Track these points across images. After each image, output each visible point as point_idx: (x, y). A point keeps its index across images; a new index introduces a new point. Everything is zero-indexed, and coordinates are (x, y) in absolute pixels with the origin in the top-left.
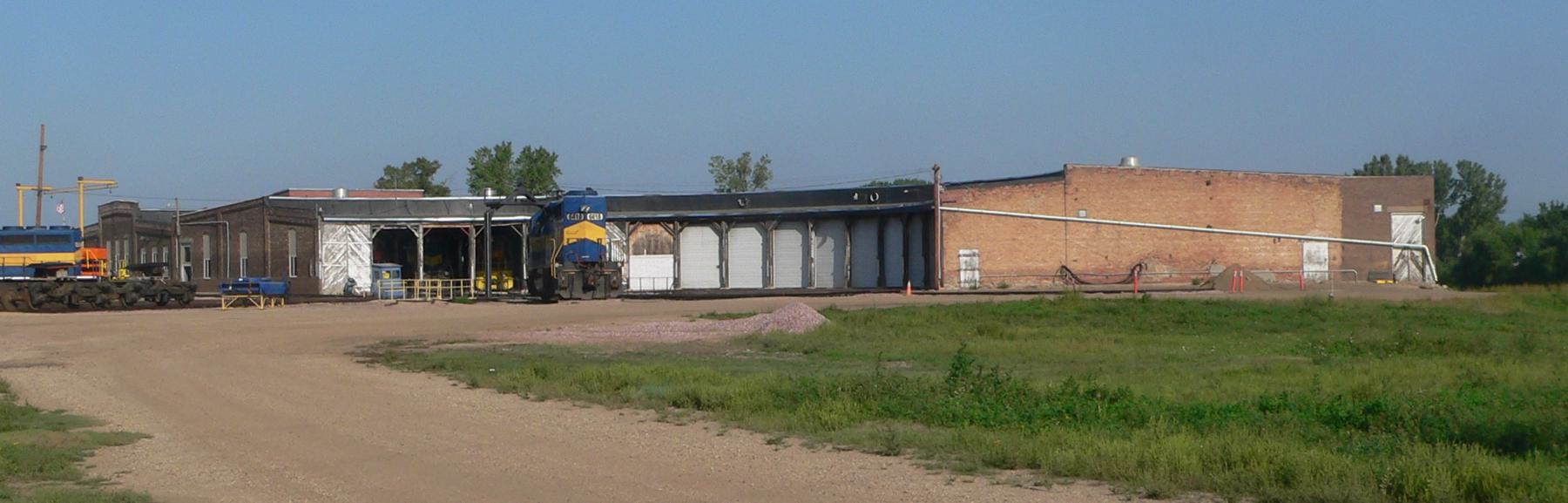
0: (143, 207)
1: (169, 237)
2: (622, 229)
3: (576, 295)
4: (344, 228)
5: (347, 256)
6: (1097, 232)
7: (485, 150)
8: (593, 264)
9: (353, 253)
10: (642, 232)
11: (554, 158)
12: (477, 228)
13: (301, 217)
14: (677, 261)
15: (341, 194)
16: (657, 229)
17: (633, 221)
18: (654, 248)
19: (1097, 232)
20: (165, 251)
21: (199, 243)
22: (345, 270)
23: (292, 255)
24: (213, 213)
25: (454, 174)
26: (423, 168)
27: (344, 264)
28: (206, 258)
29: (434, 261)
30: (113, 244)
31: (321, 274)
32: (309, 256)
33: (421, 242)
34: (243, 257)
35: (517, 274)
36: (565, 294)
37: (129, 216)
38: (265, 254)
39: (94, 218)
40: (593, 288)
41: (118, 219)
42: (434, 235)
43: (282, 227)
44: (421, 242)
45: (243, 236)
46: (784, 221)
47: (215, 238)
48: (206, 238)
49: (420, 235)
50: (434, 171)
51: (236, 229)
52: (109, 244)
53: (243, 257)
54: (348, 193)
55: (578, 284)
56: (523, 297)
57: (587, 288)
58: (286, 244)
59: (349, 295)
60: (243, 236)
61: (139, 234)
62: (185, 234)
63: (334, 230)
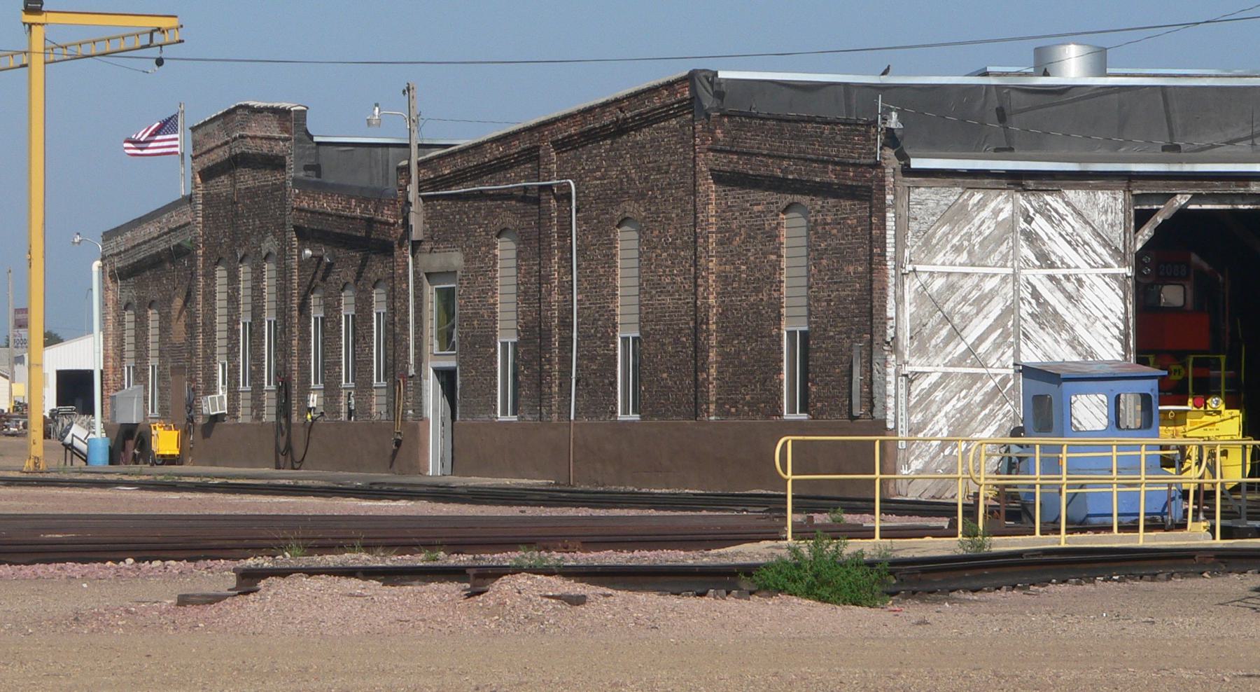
0: (323, 130)
1: (386, 249)
4: (1003, 205)
6: (1253, 144)
13: (829, 158)
15: (1072, 67)
19: (1253, 144)
20: (379, 300)
21: (482, 269)
23: (793, 323)
24: (523, 148)
28: (506, 336)
30: (233, 278)
31: (896, 406)
32: (853, 325)
34: (627, 330)
37: (275, 163)
38: (699, 320)
39: (180, 181)
41: (248, 179)
43: (761, 199)
45: (626, 242)
47: (534, 247)
48: (505, 250)
51: (604, 212)
52: (221, 273)
53: (627, 330)
60: (626, 242)
61: (305, 235)
62: (441, 235)
63: (957, 215)
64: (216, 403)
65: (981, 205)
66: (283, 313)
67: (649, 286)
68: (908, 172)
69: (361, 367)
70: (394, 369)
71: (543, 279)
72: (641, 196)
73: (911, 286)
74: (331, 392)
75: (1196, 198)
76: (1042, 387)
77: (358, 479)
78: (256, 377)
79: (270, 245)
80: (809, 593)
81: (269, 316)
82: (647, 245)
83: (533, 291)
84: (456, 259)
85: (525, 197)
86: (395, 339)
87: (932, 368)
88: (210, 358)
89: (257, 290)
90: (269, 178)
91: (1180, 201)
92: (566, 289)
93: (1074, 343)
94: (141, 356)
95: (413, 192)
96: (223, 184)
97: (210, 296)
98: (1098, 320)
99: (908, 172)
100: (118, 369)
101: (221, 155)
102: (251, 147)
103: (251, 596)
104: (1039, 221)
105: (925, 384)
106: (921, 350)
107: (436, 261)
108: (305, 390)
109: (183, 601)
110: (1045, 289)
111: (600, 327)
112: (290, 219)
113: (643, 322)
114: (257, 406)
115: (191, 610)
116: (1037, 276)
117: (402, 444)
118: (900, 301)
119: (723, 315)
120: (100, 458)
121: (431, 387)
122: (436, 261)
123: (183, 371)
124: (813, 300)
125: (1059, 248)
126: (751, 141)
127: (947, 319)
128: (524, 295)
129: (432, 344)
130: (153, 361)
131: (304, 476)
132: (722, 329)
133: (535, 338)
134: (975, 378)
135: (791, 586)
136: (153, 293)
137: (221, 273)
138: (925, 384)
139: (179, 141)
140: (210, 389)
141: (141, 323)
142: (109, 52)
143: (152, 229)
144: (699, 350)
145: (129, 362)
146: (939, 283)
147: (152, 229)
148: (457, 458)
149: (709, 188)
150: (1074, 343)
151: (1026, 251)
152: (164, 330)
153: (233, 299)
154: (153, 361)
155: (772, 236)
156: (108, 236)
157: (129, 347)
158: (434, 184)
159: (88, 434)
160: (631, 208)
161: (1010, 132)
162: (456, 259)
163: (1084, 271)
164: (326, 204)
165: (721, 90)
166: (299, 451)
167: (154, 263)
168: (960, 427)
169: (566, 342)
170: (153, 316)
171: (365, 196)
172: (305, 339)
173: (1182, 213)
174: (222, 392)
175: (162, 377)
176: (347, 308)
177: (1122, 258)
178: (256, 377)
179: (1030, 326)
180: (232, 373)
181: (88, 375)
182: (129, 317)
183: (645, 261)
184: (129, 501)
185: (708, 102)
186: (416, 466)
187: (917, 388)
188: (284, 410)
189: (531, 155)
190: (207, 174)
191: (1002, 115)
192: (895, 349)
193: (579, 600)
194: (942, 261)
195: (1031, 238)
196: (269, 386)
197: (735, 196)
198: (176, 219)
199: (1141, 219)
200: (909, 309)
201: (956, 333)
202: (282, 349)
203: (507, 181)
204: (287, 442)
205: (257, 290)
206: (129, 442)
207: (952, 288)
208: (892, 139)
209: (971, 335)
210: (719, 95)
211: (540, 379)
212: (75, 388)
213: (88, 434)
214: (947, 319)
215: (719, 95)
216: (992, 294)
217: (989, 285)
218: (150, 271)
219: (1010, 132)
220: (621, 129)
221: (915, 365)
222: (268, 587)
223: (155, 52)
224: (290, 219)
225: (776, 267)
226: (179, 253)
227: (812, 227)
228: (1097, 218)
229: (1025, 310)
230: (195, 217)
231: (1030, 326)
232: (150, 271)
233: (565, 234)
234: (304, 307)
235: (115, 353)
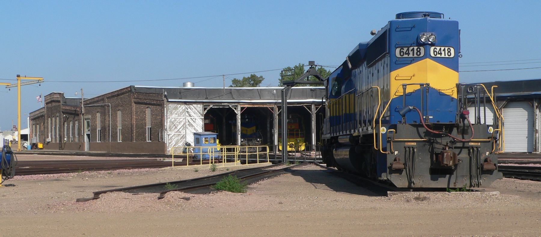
1: (78, 115)
3: (418, 182)
4: (183, 107)
5: (184, 126)
8: (450, 128)
9: (191, 125)
12: (279, 108)
13: (154, 100)
15: (189, 86)
20: (77, 123)
21: (94, 118)
22: (184, 137)
23: (148, 126)
24: (101, 98)
25: (272, 83)
26: (254, 80)
27: (183, 132)
28: (99, 128)
29: (250, 131)
30: (52, 120)
31: (166, 140)
32: (159, 126)
33: (239, 117)
34: (119, 127)
35: (308, 140)
36: (399, 181)
37: (59, 102)
38: (132, 125)
39: (42, 105)
40: (446, 171)
41: (54, 104)
42: (246, 112)
43: (143, 106)
44: (239, 117)
45: (119, 113)
46: (510, 102)
47: (103, 114)
48: (98, 115)
49: (238, 112)
50: (260, 82)
51: (115, 109)
52: (49, 119)
53: (119, 127)
54: (193, 85)
55: (423, 163)
57: (439, 170)
58: (144, 119)
60: (119, 113)
62: (87, 113)
63: (176, 108)
64: (49, 140)
65: (180, 107)
66: (60, 125)
67: (123, 120)
68: (168, 101)
69: (73, 134)
70: (79, 134)
71: (105, 119)
72: (122, 106)
73: (169, 120)
74: (68, 137)
75: (214, 106)
76: (197, 136)
77: (74, 152)
78: (55, 135)
79: (58, 114)
80: (229, 190)
81: (58, 126)
82: (123, 114)
83: (103, 121)
84: (90, 116)
85: (102, 106)
86: (79, 129)
87: (173, 133)
88: (48, 133)
89: (56, 122)
90: (57, 104)
91: (211, 106)
92: (109, 121)
93: (195, 129)
94: (36, 132)
95: (82, 106)
96: (50, 105)
97: (48, 123)
98: (199, 125)
99: (168, 101)
100: (32, 134)
101: (49, 100)
102: (54, 99)
103: (98, 200)
104: (189, 110)
105: (171, 136)
106: (170, 130)
107: (86, 117)
108: (64, 137)
109: (78, 200)
110: (190, 121)
111: (115, 127)
112: (61, 110)
113: (122, 126)
114: (56, 140)
115: (80, 203)
116: (189, 118)
117: (81, 146)
118: (167, 122)
119: (136, 125)
120: (29, 148)
121: (86, 136)
122: (86, 117)
123: (43, 135)
124: (152, 122)
125: (192, 114)
126: (141, 97)
127: (175, 125)
128: (101, 122)
129: (86, 130)
130: (38, 133)
131: (62, 152)
132: (136, 127)
133: (104, 130)
134: (179, 135)
135: (224, 189)
136: (38, 122)
137: (49, 119)
138: (171, 136)
139: (43, 99)
140: (48, 137)
141: (36, 127)
142: (31, 83)
143: (38, 112)
144: (132, 131)
145: (34, 133)
146: (173, 119)
147: (38, 112)
148: (90, 148)
149: (134, 104)
150: (195, 129)
151: (187, 114)
152: (40, 128)
153: (51, 123)
154: (38, 133)
155: (145, 112)
156: (30, 114)
157: (34, 131)
158: (86, 104)
159: (27, 144)
160: (120, 108)
161: (183, 96)
162: (90, 116)
163: (196, 117)
164: (67, 108)
165: (135, 89)
166: (63, 147)
167: (38, 118)
168: (177, 143)
169: (109, 130)
170: (38, 126)
171: (74, 107)
172: (64, 129)
173: (211, 108)
174: (50, 138)
175: (39, 135)
176: (71, 125)
177: (202, 115)
178: (55, 135)
179: (188, 126)
180: (52, 135)
181: (27, 135)
182: (34, 126)
183: (123, 116)
184: (36, 158)
185: (133, 91)
186: (83, 149)
187: (170, 137)
188: (60, 141)
189: (103, 100)
190: (47, 104)
191: (180, 93)
192: (166, 130)
193: (188, 199)
194: (173, 116)
195: (188, 112)
196: (58, 137)
197: (138, 106)
198: (42, 111)
199: (205, 109)
200: (168, 124)
201: (176, 128)
202: (60, 131)
203: (98, 104)
204: (61, 145)
205: (56, 122)
206: (34, 146)
207: (175, 120)
208: (165, 96)
209: (178, 128)
210: (135, 89)
211: (105, 136)
212: (24, 137)
213: (27, 144)
214: (175, 125)
215: (135, 89)
216: (182, 121)
217: (181, 120)
218: (37, 119)
219: (183, 96)
220: (118, 95)
221: (169, 133)
222: (102, 196)
223: (39, 84)
224: (61, 110)
225: (145, 117)
226: (42, 116)
227: (152, 111)
228: (198, 109)
229: (187, 124)
230: (45, 110)
231: (188, 126)
232: (37, 119)
233: (109, 112)
234: (64, 124)
235: (32, 132)
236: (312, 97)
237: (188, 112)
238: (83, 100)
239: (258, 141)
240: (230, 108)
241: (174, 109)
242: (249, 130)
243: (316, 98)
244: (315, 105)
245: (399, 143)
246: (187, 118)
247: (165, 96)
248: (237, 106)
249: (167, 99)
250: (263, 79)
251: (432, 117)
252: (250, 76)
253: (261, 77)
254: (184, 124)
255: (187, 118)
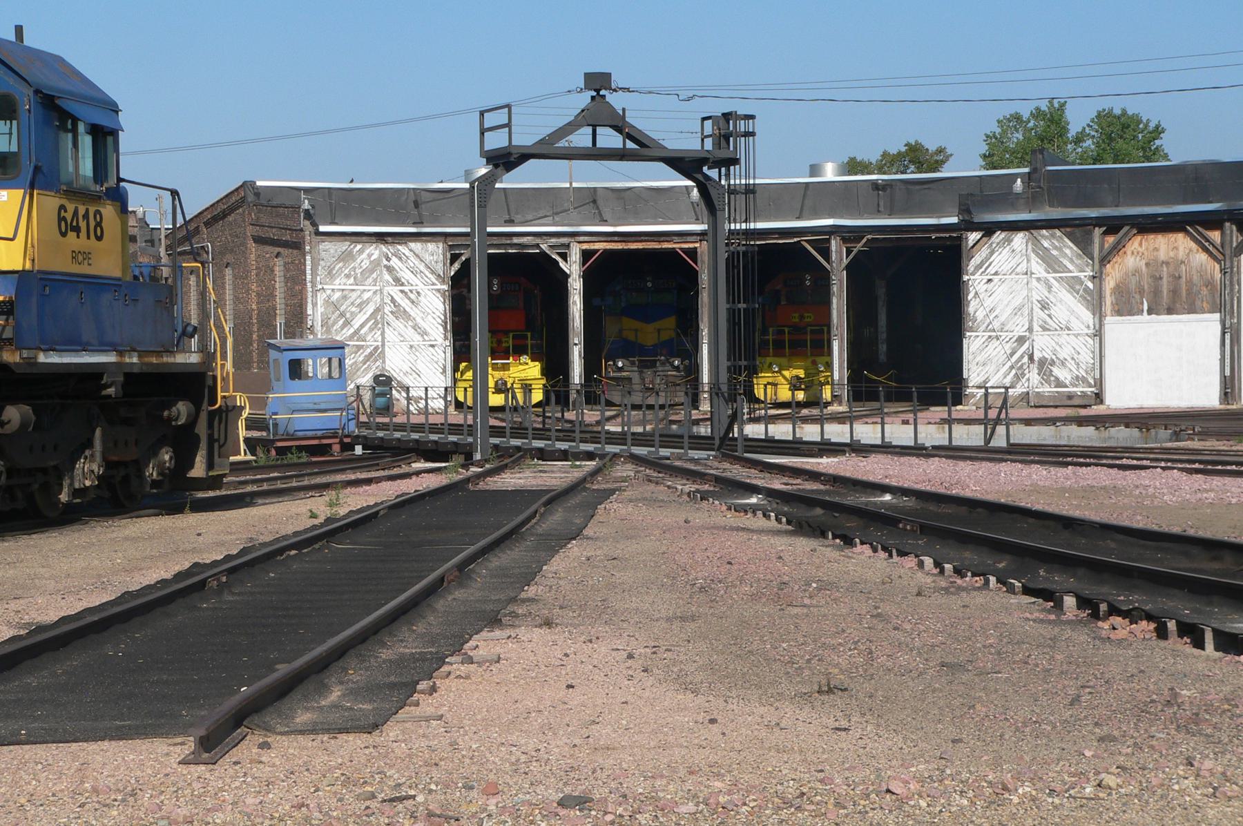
2: (1084, 245)
4: (375, 251)
7: (1017, 118)
9: (400, 313)
10: (1140, 254)
11: (1158, 131)
14: (1229, 332)
16: (1176, 247)
17: (1112, 226)
18: (1169, 297)
27: (373, 340)
33: (576, 286)
44: (576, 286)
49: (573, 268)
56: (360, 459)
59: (383, 440)
63: (346, 257)
65: (361, 252)
68: (318, 233)
72: (232, 251)
73: (321, 298)
104: (395, 262)
110: (399, 298)
116: (394, 291)
118: (315, 305)
125: (406, 275)
126: (265, 220)
127: (342, 315)
134: (359, 348)
146: (337, 295)
149: (251, 244)
151: (387, 277)
163: (421, 287)
185: (251, 198)
194: (339, 283)
195: (390, 269)
199: (454, 258)
200: (320, 309)
201: (347, 323)
207: (345, 298)
208: (308, 215)
209: (357, 323)
210: (257, 194)
214: (342, 315)
216: (368, 301)
217: (366, 296)
220: (224, 215)
228: (428, 258)
229: (387, 309)
231: (391, 318)
236: (878, 213)
237: (390, 269)
238: (163, 233)
239: (677, 369)
240: (543, 254)
241: (340, 259)
242: (651, 328)
243: (891, 213)
244: (844, 240)
245: (381, 401)
246: (388, 289)
247: (308, 215)
248: (568, 246)
249: (314, 225)
250: (948, 157)
251: (808, 283)
252: (904, 149)
253: (940, 151)
254: (377, 310)
255: (388, 289)
